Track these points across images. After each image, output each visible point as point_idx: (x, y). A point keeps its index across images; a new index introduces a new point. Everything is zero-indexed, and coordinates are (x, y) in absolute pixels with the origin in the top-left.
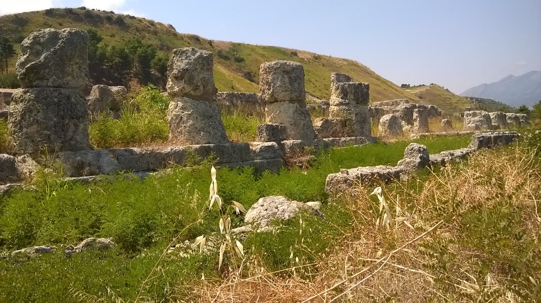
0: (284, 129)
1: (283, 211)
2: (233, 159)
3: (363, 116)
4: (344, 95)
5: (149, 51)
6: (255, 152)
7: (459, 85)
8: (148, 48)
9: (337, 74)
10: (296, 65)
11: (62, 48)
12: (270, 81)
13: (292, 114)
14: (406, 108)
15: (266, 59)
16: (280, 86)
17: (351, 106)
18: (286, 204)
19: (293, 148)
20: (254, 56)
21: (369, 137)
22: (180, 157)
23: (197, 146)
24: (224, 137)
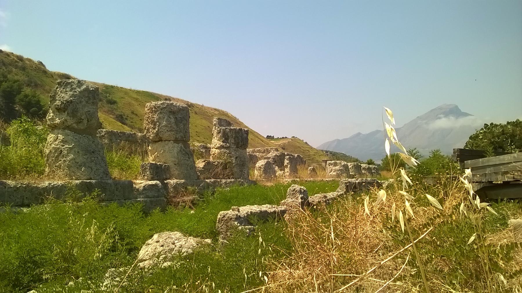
0: (168, 168)
1: (180, 247)
2: (115, 197)
3: (243, 160)
4: (226, 139)
5: (15, 86)
6: (138, 190)
7: (316, 139)
8: (14, 83)
9: (219, 119)
10: (182, 107)
12: (156, 120)
13: (176, 154)
15: (139, 103)
16: (166, 126)
17: (232, 149)
18: (184, 240)
19: (176, 187)
20: (127, 99)
21: (247, 179)
22: (59, 192)
23: (78, 182)
24: (107, 174)
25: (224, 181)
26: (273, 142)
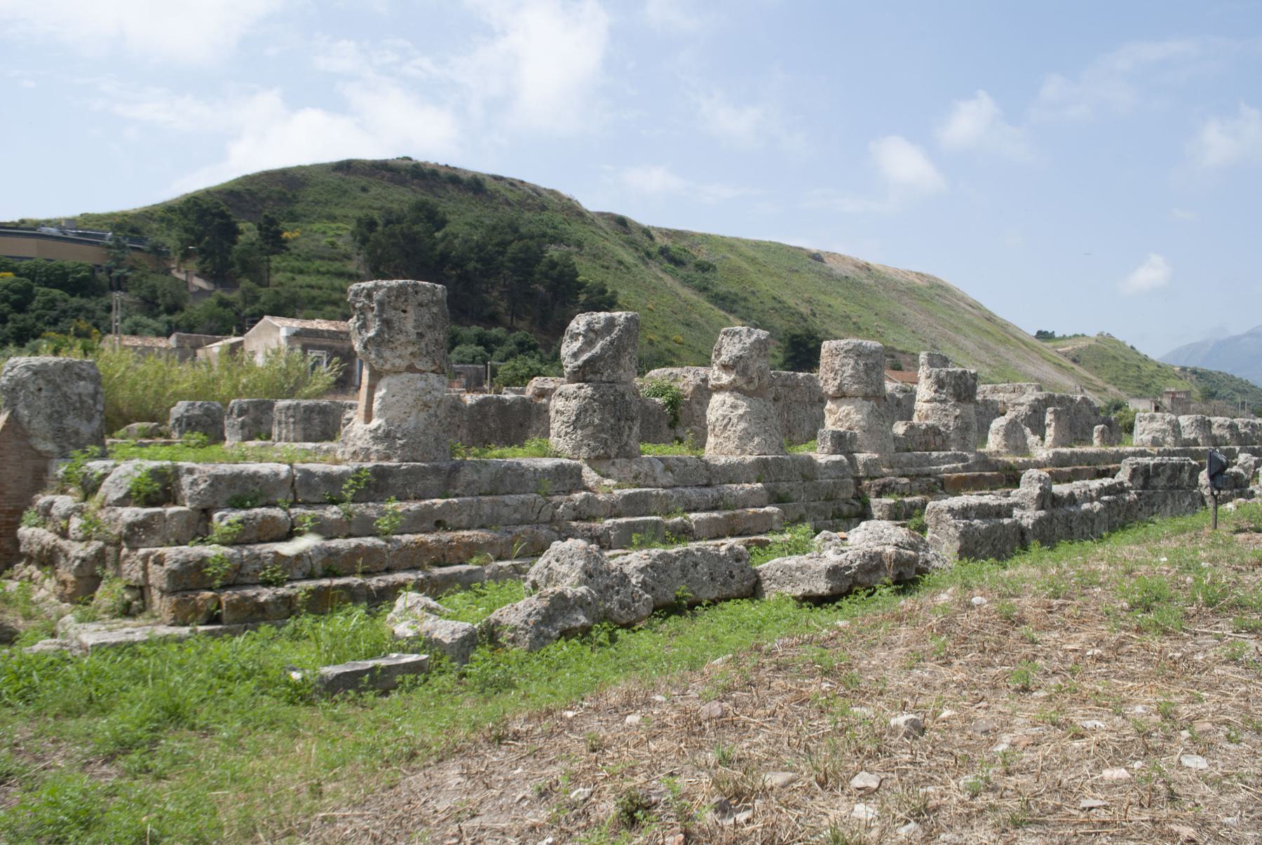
11: (619, 338)
14: (1037, 400)
16: (851, 376)
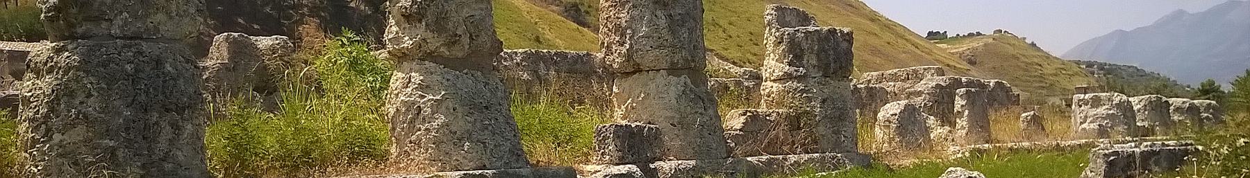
0: (656, 135)
4: (795, 56)
9: (778, 9)
16: (647, 37)
17: (812, 81)
21: (852, 153)
24: (517, 154)
25: (793, 158)
26: (945, 46)
